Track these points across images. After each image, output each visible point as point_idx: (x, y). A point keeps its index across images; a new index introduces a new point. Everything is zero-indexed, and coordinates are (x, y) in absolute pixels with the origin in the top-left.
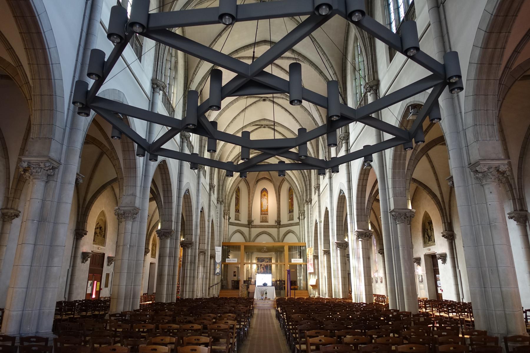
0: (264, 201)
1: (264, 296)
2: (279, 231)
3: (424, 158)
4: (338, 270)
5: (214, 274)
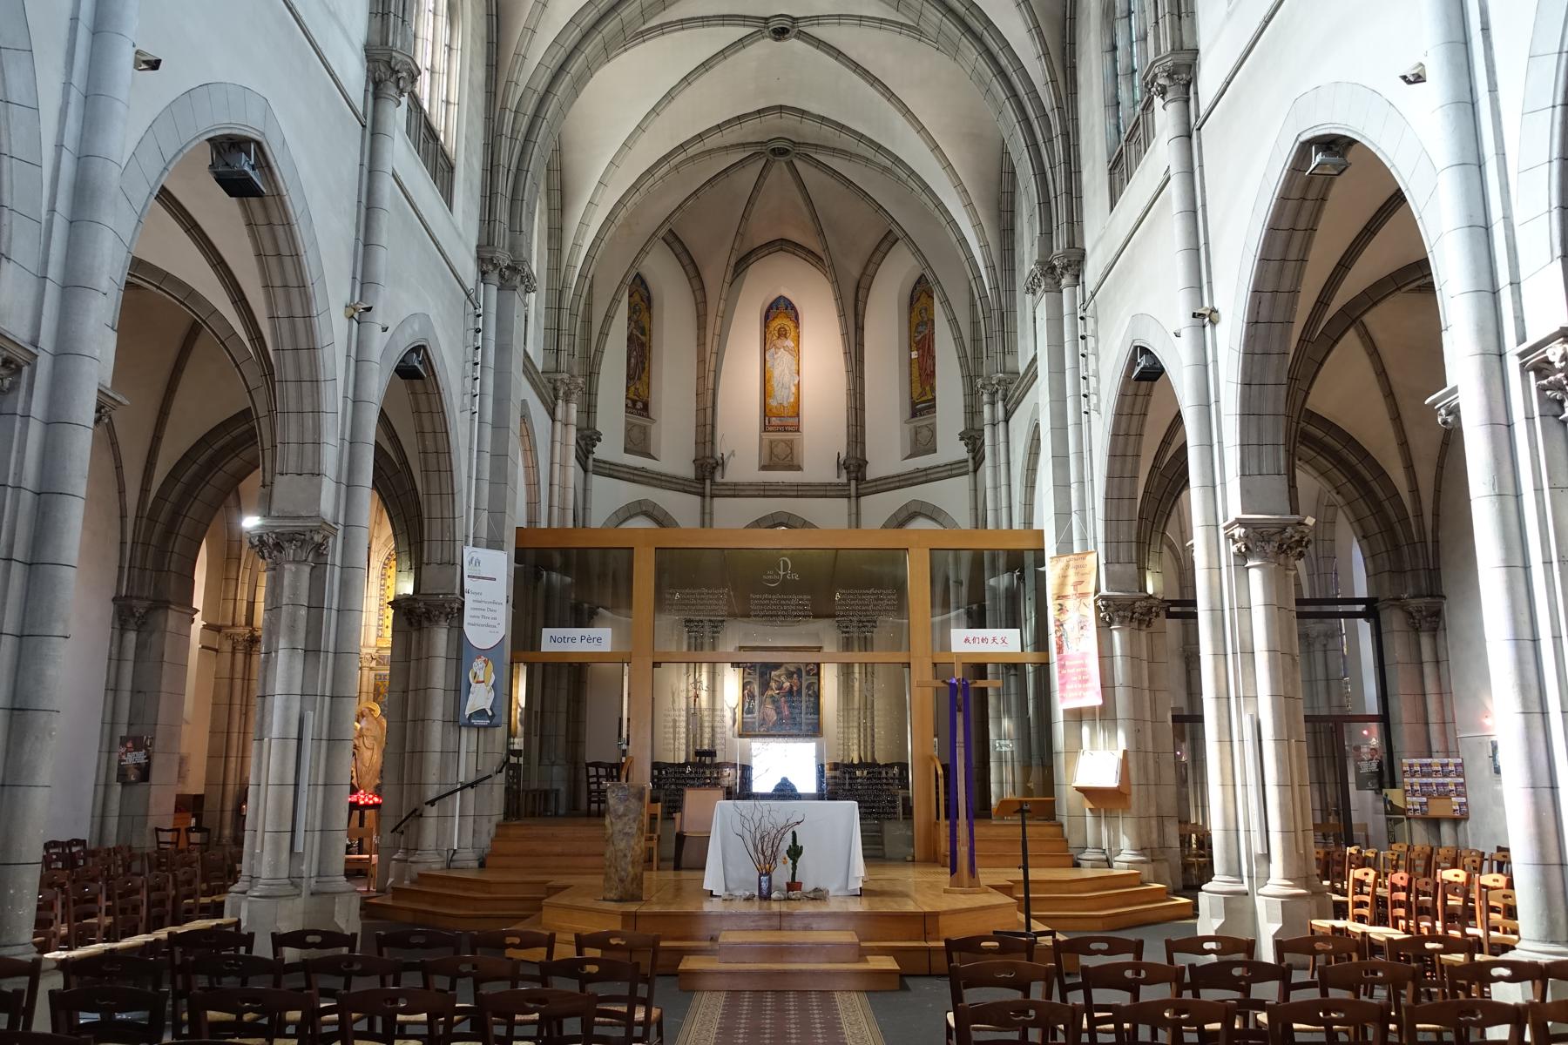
0: (782, 363)
1: (782, 874)
3: (1351, 337)
4: (1223, 698)
5: (456, 721)
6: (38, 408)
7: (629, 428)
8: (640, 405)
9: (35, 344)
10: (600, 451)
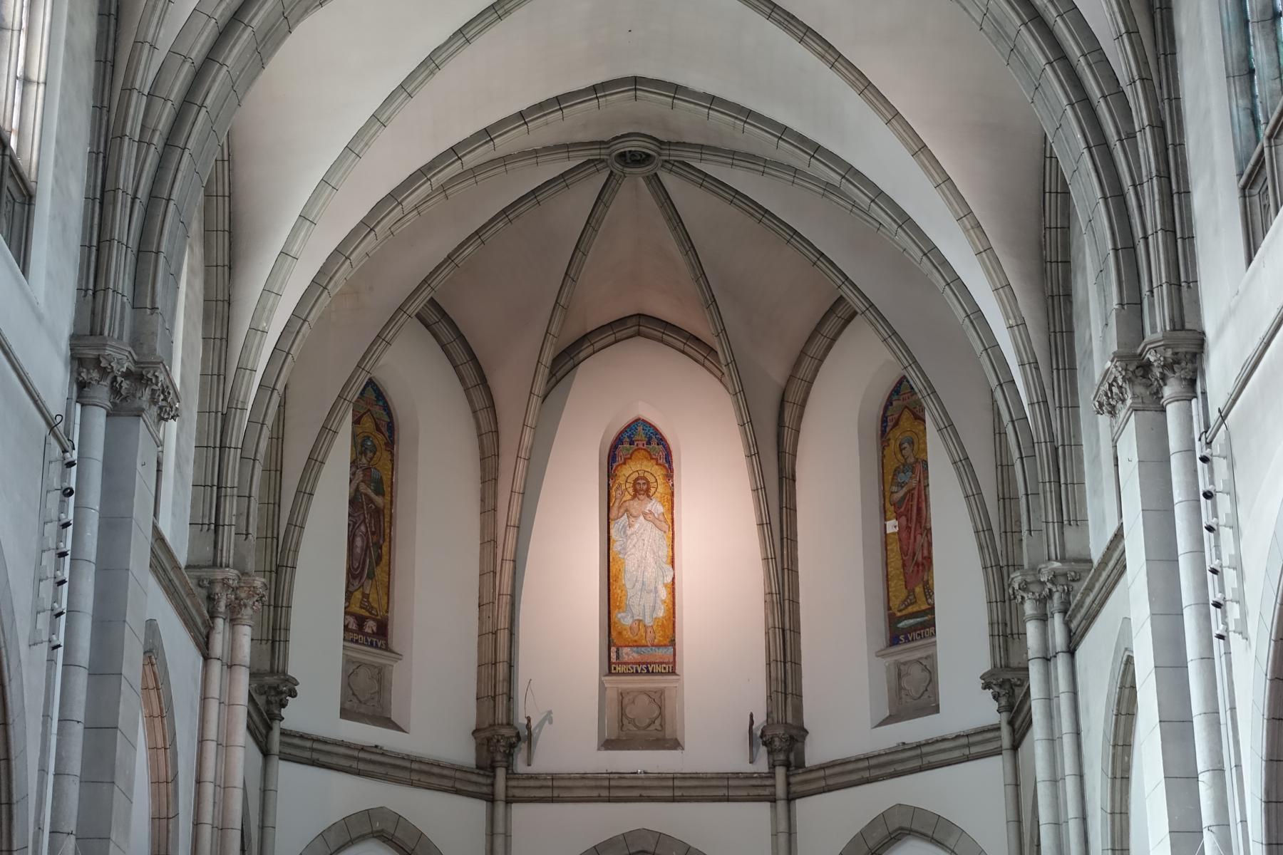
0: (641, 544)
7: (351, 671)
8: (370, 626)
10: (295, 716)
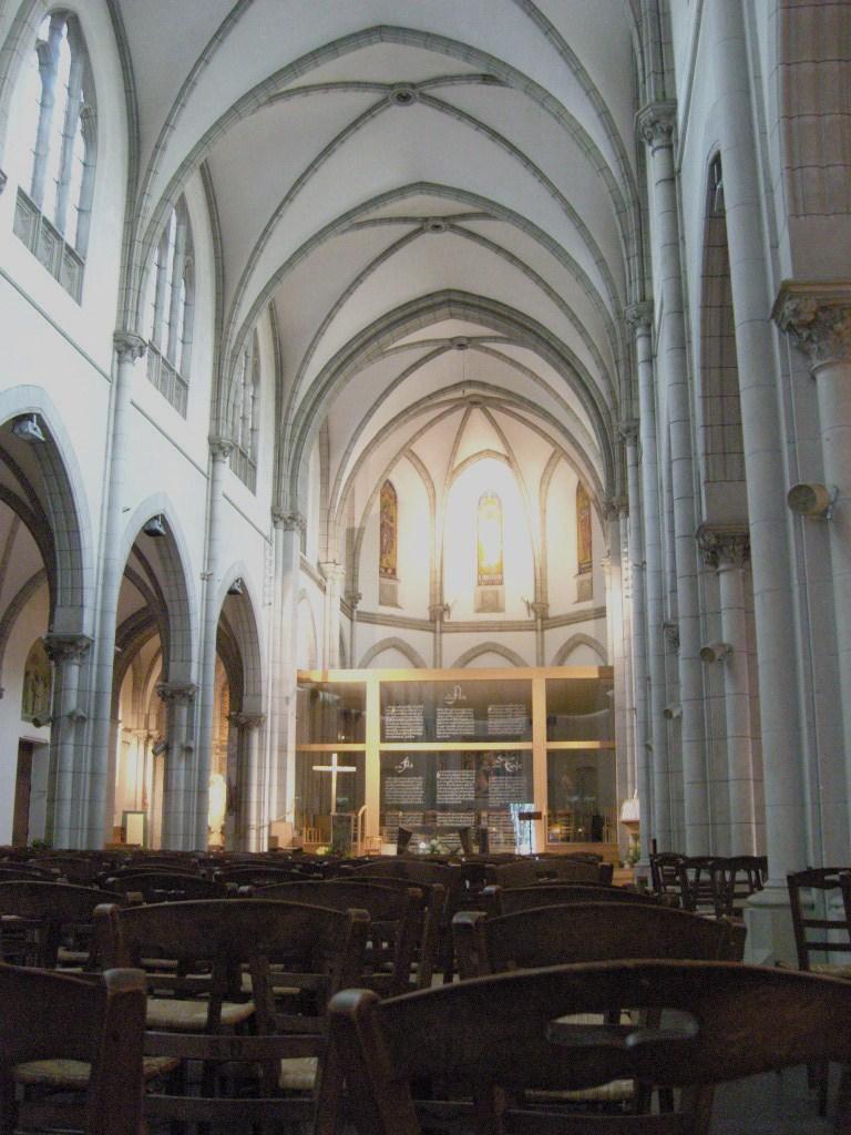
2: (541, 644)
6: (95, 662)
7: (382, 587)
8: (390, 571)
9: (93, 635)
10: (361, 606)
